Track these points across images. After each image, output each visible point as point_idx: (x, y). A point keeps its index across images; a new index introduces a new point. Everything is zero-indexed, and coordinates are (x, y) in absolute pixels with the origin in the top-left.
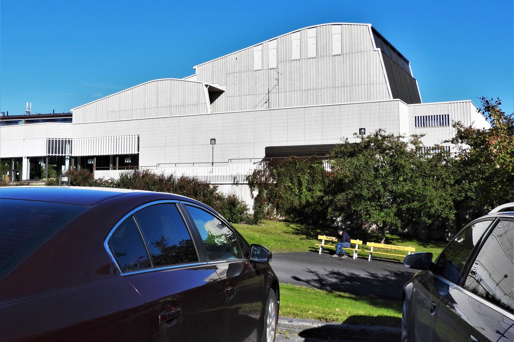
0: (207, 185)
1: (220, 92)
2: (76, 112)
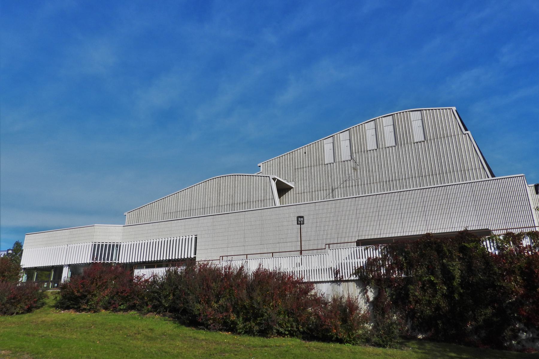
0: (299, 282)
1: (290, 188)
2: (130, 215)
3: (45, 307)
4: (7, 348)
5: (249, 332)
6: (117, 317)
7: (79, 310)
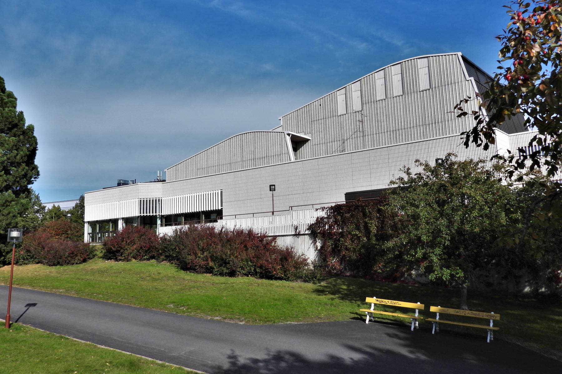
3: (96, 257)
4: (63, 288)
5: (222, 274)
6: (141, 265)
7: (117, 260)
